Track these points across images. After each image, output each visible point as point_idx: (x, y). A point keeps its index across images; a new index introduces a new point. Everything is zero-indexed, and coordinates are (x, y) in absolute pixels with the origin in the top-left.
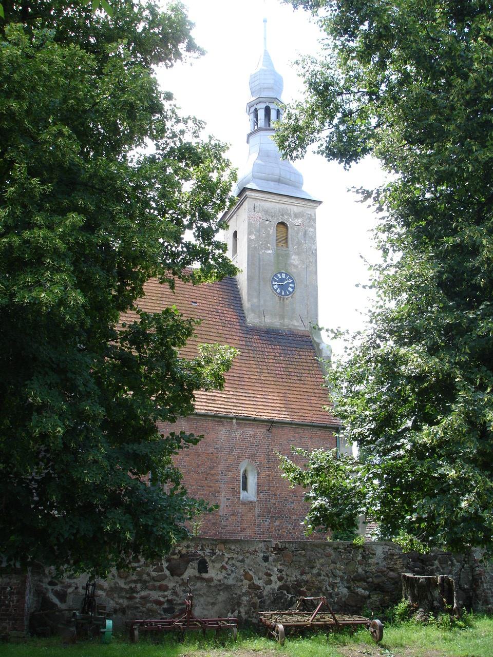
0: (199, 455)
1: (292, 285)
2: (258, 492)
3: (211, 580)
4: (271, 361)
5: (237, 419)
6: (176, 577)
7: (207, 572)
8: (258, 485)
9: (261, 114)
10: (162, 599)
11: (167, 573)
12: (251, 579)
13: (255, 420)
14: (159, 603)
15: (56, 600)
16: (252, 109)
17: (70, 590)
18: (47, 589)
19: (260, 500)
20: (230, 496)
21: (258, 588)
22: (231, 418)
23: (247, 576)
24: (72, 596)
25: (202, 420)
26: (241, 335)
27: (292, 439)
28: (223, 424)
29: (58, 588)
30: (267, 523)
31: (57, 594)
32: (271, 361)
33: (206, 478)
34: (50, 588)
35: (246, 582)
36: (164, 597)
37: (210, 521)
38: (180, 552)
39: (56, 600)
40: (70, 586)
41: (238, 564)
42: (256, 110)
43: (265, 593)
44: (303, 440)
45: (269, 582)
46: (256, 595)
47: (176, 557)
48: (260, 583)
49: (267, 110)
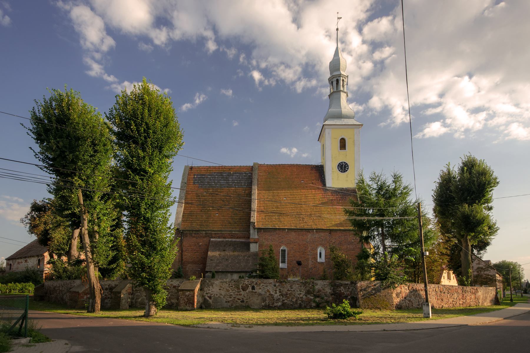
0: (300, 245)
1: (347, 167)
2: (326, 258)
3: (256, 292)
4: (335, 203)
5: (316, 230)
6: (244, 292)
7: (254, 290)
8: (326, 256)
9: (335, 83)
10: (240, 298)
11: (242, 290)
12: (270, 292)
13: (323, 229)
14: (239, 299)
15: (208, 299)
16: (331, 81)
17: (212, 296)
18: (205, 296)
19: (326, 261)
20: (313, 260)
21: (272, 295)
22: (313, 230)
23: (268, 291)
24: (213, 297)
25: (301, 231)
26: (322, 193)
27: (341, 236)
28: (310, 233)
29: (209, 295)
30: (329, 271)
31: (208, 297)
32: (335, 203)
33: (303, 254)
34: (206, 295)
35: (268, 293)
36: (240, 297)
37: (305, 270)
38: (245, 284)
39: (208, 299)
40: (212, 294)
41: (265, 287)
42: (332, 82)
43: (274, 297)
44: (346, 236)
45: (276, 293)
46: (272, 297)
47: (244, 285)
48: (273, 293)
49: (338, 81)
